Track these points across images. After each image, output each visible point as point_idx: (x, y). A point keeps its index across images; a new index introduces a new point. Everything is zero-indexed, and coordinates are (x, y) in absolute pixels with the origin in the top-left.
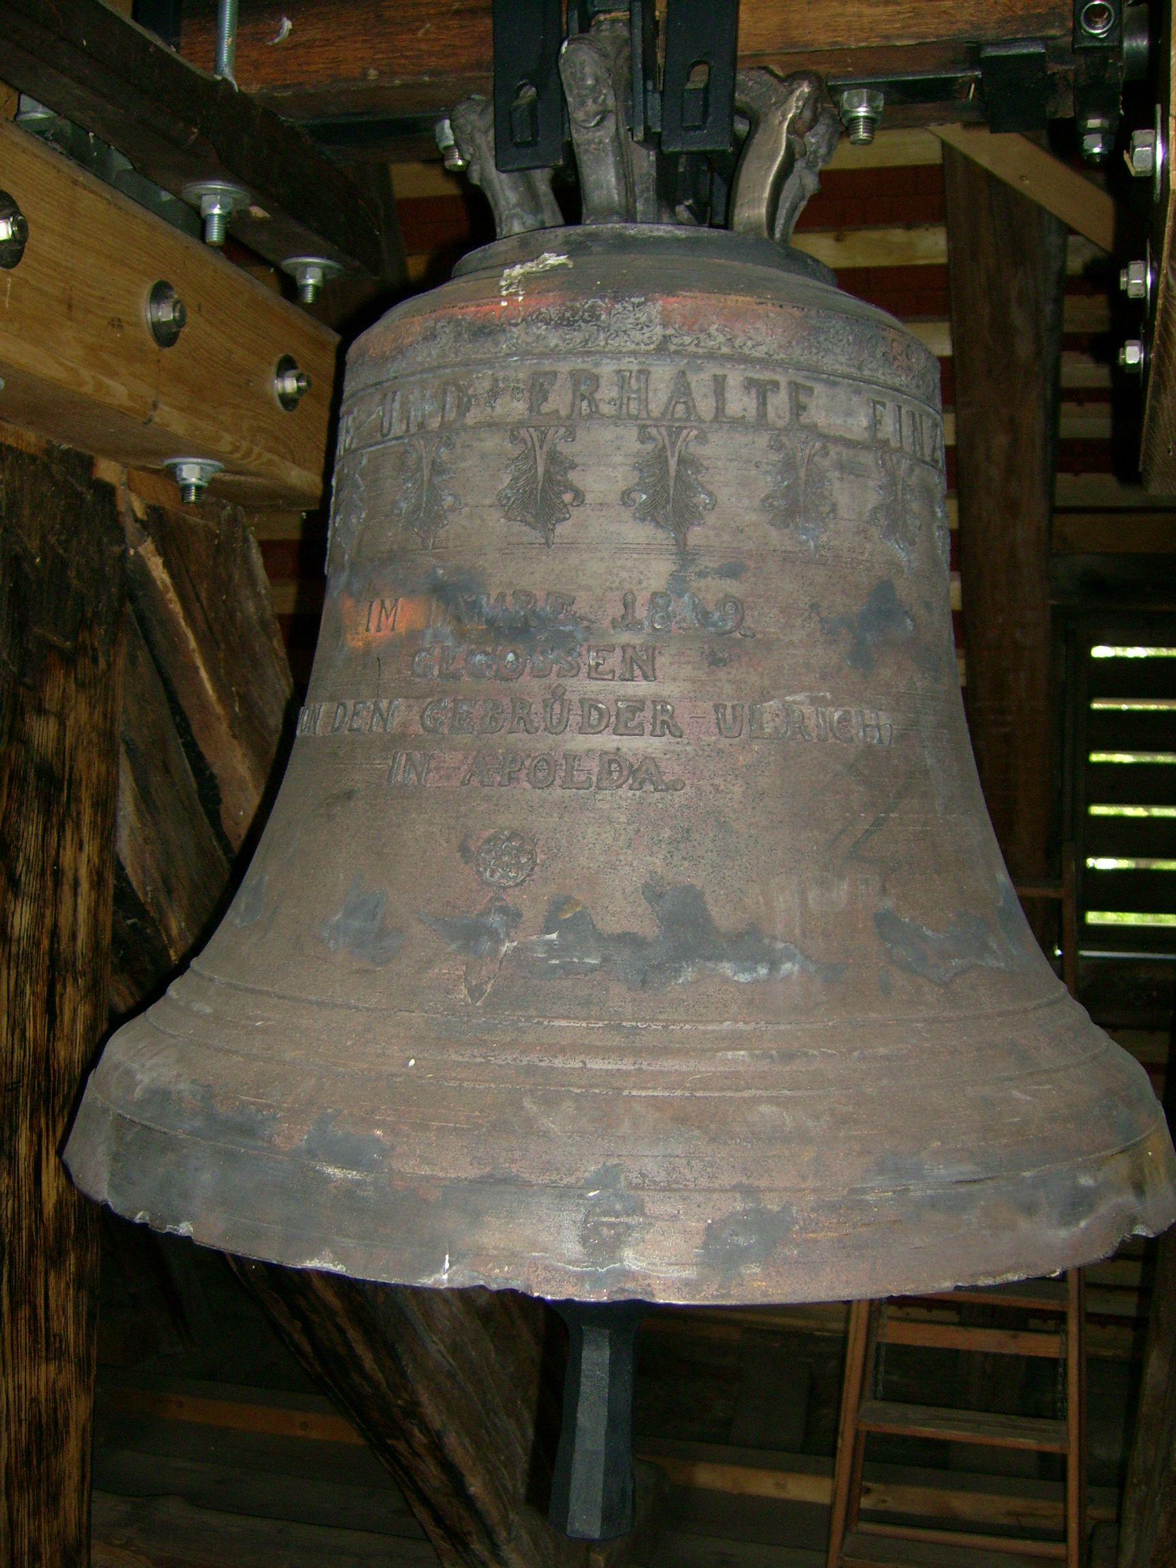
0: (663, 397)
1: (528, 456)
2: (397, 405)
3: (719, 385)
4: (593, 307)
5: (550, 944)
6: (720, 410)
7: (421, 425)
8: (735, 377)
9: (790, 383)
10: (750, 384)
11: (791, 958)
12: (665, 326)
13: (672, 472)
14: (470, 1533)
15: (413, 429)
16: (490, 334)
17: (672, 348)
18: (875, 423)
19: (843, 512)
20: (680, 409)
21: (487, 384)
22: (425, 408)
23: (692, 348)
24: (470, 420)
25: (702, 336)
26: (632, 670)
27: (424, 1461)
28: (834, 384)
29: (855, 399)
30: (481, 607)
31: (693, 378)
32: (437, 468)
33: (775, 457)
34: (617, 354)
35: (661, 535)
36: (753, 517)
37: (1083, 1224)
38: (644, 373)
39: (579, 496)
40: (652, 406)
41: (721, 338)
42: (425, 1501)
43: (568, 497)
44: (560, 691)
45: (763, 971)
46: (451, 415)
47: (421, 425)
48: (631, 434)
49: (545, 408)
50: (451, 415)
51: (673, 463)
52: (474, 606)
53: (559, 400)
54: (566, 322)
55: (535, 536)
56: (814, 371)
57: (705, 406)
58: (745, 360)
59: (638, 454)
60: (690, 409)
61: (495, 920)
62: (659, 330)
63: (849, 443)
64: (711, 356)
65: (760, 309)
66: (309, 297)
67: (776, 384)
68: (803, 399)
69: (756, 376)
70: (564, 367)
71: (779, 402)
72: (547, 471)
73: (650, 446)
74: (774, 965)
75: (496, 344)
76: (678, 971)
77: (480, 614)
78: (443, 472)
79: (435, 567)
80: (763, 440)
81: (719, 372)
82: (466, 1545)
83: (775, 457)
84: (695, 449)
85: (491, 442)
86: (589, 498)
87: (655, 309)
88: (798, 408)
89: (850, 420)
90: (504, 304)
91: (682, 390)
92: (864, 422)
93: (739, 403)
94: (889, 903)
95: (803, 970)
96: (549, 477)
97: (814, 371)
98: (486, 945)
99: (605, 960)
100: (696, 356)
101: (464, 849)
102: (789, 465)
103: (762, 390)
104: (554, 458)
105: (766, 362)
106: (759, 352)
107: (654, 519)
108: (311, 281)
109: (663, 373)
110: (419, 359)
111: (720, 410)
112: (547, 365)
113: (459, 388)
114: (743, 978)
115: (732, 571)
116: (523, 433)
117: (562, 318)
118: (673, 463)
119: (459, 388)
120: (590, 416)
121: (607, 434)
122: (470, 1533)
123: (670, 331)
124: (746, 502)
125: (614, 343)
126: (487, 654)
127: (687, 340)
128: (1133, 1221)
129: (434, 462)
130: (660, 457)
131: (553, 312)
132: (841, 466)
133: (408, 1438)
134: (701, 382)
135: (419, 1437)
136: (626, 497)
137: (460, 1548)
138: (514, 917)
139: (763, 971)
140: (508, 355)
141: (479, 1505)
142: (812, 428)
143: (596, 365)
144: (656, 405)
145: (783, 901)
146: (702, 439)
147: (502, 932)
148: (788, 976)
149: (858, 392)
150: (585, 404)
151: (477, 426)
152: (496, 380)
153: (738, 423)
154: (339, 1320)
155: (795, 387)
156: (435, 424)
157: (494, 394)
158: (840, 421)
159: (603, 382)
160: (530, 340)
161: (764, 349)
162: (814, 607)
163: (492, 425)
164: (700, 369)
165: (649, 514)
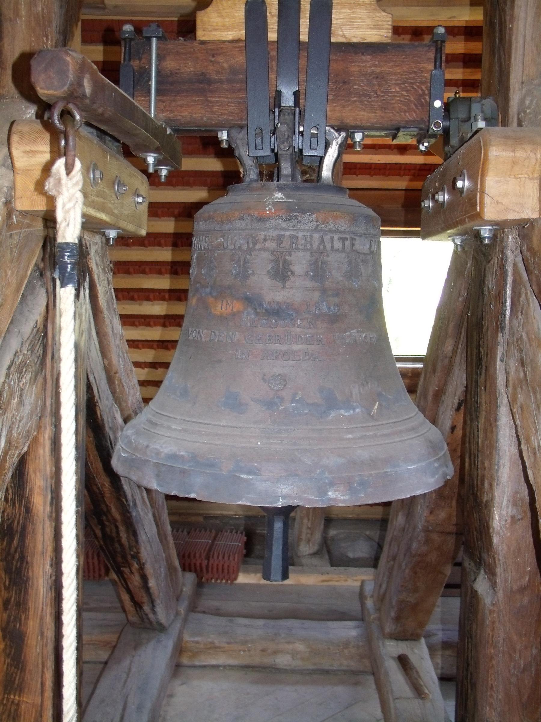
0: (317, 244)
1: (277, 261)
2: (229, 239)
3: (332, 238)
4: (296, 216)
5: (293, 406)
6: (332, 247)
7: (240, 247)
8: (336, 237)
9: (350, 238)
10: (340, 239)
11: (358, 407)
12: (317, 222)
13: (320, 266)
14: (144, 603)
15: (237, 248)
16: (264, 221)
17: (319, 229)
18: (371, 247)
19: (364, 275)
20: (322, 247)
21: (263, 237)
22: (241, 242)
23: (324, 229)
24: (257, 247)
25: (327, 225)
26: (310, 325)
27: (134, 575)
28: (361, 236)
29: (366, 240)
30: (263, 305)
31: (325, 238)
32: (246, 262)
33: (347, 260)
34: (303, 230)
35: (316, 284)
36: (341, 279)
37: (437, 477)
38: (311, 237)
39: (293, 273)
40: (313, 246)
41: (332, 225)
42: (129, 591)
43: (289, 273)
44: (289, 332)
45: (352, 412)
46: (251, 245)
47: (240, 247)
48: (308, 253)
49: (282, 246)
50: (251, 245)
51: (320, 263)
52: (261, 305)
53: (286, 244)
54: (288, 220)
55: (280, 284)
56: (356, 234)
57: (328, 246)
58: (340, 232)
59: (310, 261)
60: (324, 247)
61: (276, 400)
62: (315, 223)
63: (364, 254)
64: (330, 231)
65: (343, 216)
66: (163, 179)
67: (346, 239)
68: (354, 242)
69: (342, 236)
70: (288, 233)
71: (348, 243)
72: (283, 265)
73: (313, 258)
74: (354, 410)
75: (265, 224)
76: (330, 414)
77: (263, 307)
78: (248, 263)
79: (246, 292)
80: (344, 255)
81: (332, 235)
82: (141, 607)
83: (347, 260)
84: (326, 259)
85: (265, 255)
86: (296, 274)
87: (314, 216)
88: (353, 245)
89: (365, 247)
90: (268, 212)
91: (322, 241)
92: (368, 247)
93: (338, 245)
94: (380, 389)
95: (362, 411)
96: (284, 268)
97: (356, 234)
98: (275, 407)
99: (310, 411)
100: (326, 231)
101: (263, 379)
102: (350, 263)
103: (344, 240)
104: (285, 261)
105: (344, 232)
106: (342, 229)
107: (315, 280)
108: (163, 174)
109: (316, 236)
110: (238, 226)
111: (332, 247)
112: (282, 233)
113: (253, 237)
114: (347, 414)
115: (337, 295)
116: (275, 253)
117: (287, 218)
118: (320, 263)
119: (253, 237)
120: (296, 249)
121: (301, 254)
122: (144, 603)
123: (319, 223)
124: (339, 274)
125: (302, 227)
126: (266, 320)
127: (323, 226)
128: (446, 475)
129: (245, 259)
130: (316, 262)
131: (284, 216)
132: (363, 261)
133: (130, 566)
134: (327, 238)
135: (136, 566)
136: (307, 274)
137: (138, 609)
138: (282, 399)
139: (352, 412)
140: (269, 229)
141: (151, 591)
142: (356, 251)
143: (297, 233)
144: (315, 246)
145: (355, 391)
146: (328, 256)
147: (279, 404)
148: (358, 413)
149: (366, 238)
150: (294, 245)
151: (260, 250)
152: (265, 236)
153: (337, 251)
154: (117, 524)
155: (352, 239)
156: (245, 247)
157: (265, 240)
158: (362, 248)
159: (299, 239)
160: (277, 224)
161: (344, 228)
162: (357, 304)
163: (265, 250)
164: (327, 235)
165: (313, 278)
